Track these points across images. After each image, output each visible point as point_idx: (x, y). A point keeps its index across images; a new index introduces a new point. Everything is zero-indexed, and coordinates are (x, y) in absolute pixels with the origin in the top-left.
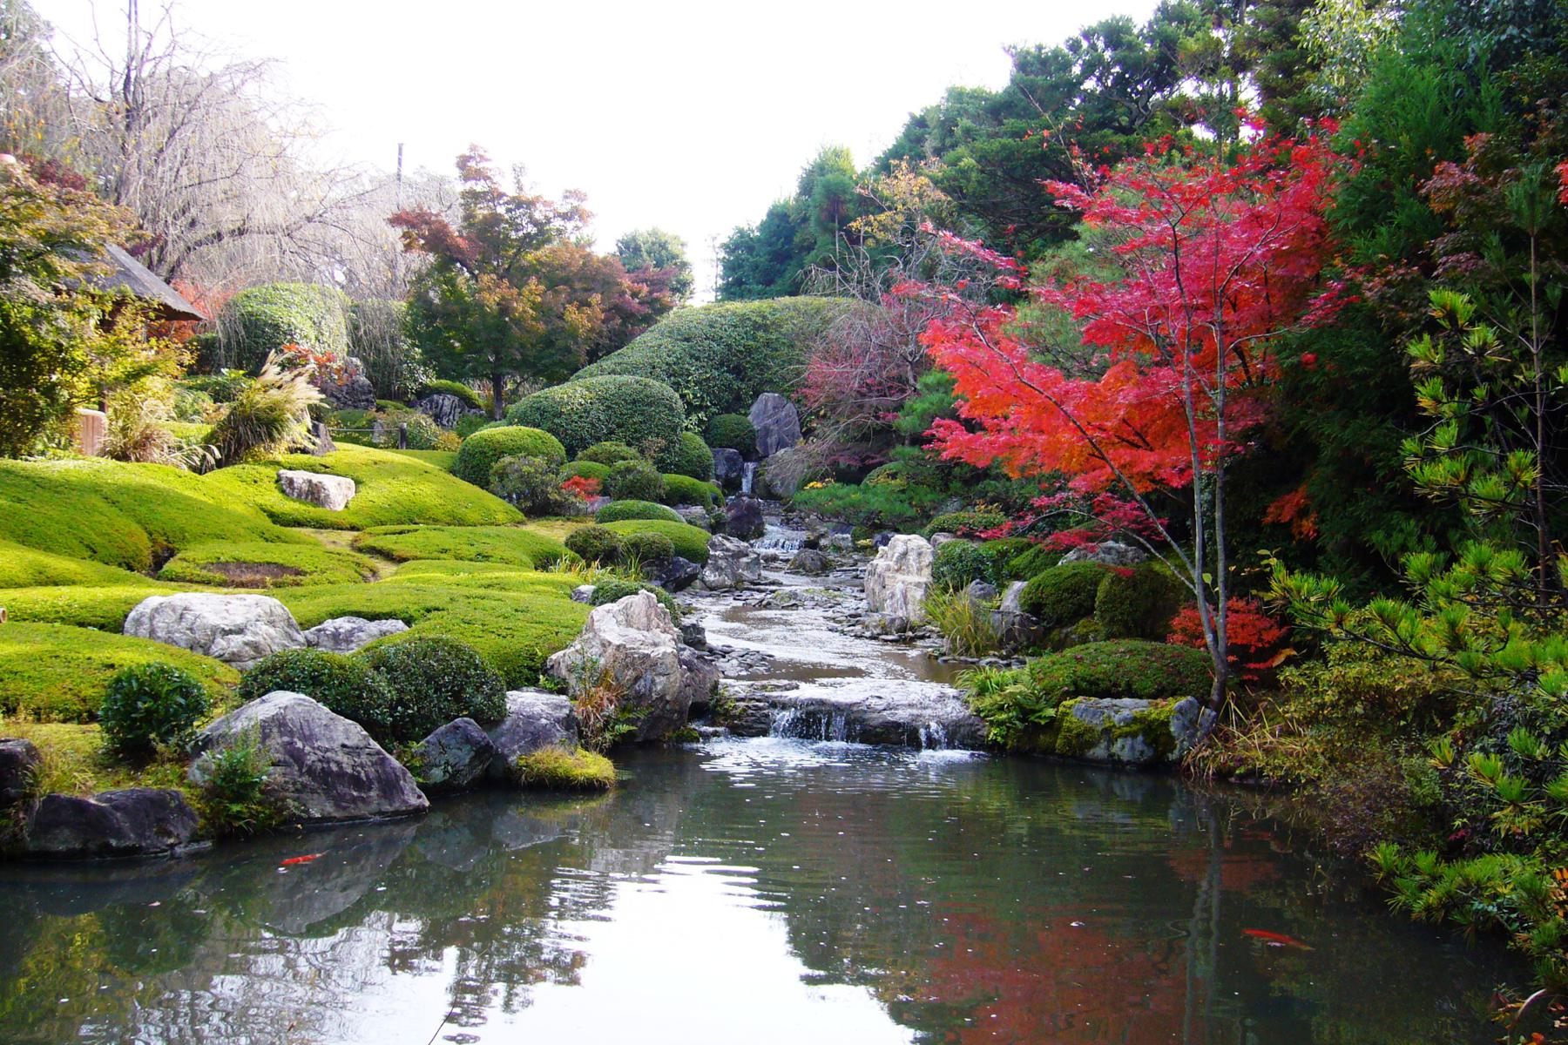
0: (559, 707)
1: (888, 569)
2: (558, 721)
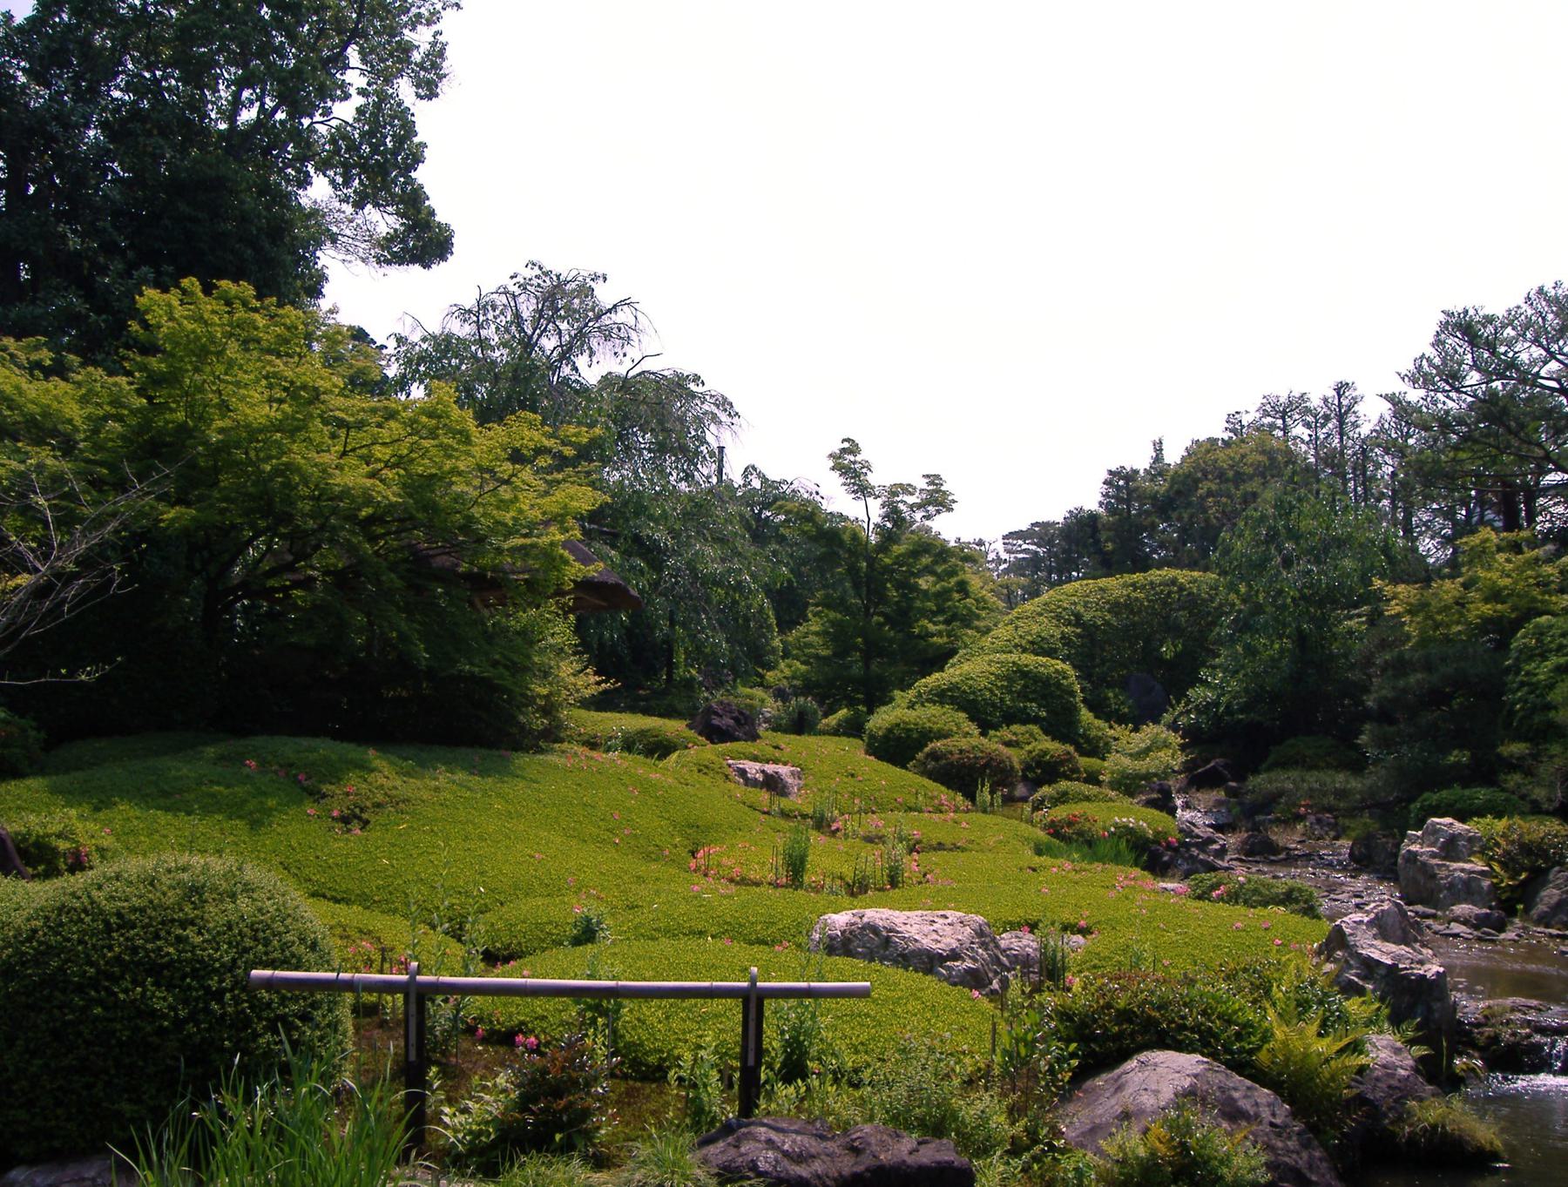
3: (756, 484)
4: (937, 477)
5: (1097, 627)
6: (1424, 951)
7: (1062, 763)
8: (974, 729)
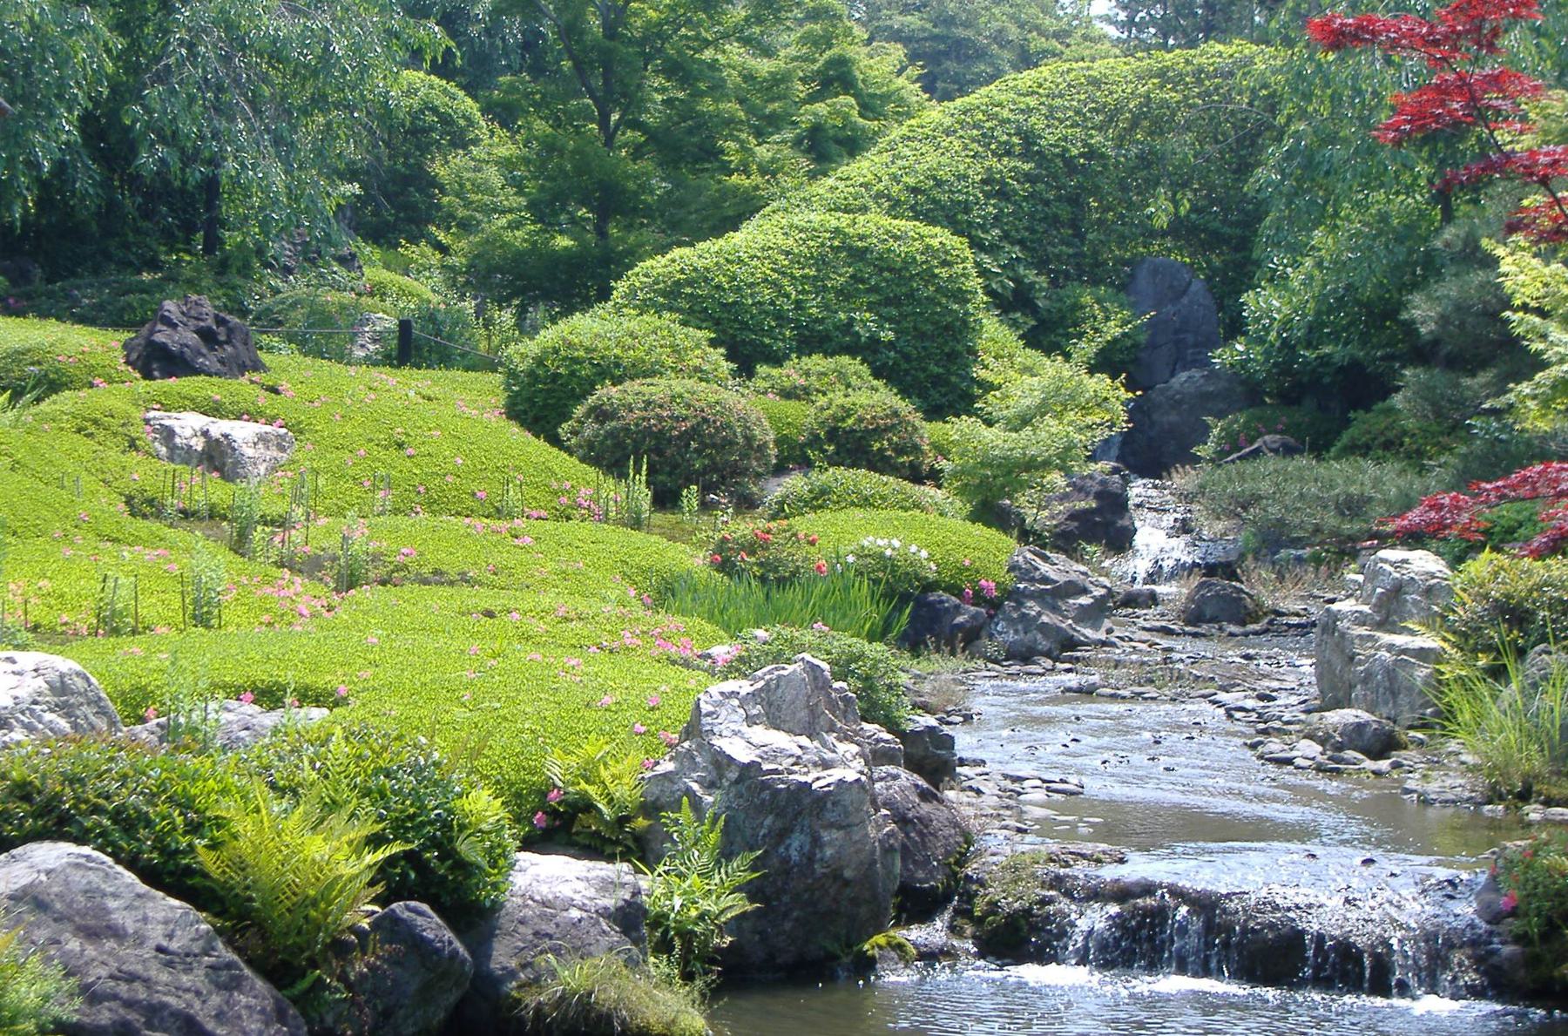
0: (607, 886)
1: (1361, 620)
2: (605, 913)
5: (1069, 162)
7: (879, 432)
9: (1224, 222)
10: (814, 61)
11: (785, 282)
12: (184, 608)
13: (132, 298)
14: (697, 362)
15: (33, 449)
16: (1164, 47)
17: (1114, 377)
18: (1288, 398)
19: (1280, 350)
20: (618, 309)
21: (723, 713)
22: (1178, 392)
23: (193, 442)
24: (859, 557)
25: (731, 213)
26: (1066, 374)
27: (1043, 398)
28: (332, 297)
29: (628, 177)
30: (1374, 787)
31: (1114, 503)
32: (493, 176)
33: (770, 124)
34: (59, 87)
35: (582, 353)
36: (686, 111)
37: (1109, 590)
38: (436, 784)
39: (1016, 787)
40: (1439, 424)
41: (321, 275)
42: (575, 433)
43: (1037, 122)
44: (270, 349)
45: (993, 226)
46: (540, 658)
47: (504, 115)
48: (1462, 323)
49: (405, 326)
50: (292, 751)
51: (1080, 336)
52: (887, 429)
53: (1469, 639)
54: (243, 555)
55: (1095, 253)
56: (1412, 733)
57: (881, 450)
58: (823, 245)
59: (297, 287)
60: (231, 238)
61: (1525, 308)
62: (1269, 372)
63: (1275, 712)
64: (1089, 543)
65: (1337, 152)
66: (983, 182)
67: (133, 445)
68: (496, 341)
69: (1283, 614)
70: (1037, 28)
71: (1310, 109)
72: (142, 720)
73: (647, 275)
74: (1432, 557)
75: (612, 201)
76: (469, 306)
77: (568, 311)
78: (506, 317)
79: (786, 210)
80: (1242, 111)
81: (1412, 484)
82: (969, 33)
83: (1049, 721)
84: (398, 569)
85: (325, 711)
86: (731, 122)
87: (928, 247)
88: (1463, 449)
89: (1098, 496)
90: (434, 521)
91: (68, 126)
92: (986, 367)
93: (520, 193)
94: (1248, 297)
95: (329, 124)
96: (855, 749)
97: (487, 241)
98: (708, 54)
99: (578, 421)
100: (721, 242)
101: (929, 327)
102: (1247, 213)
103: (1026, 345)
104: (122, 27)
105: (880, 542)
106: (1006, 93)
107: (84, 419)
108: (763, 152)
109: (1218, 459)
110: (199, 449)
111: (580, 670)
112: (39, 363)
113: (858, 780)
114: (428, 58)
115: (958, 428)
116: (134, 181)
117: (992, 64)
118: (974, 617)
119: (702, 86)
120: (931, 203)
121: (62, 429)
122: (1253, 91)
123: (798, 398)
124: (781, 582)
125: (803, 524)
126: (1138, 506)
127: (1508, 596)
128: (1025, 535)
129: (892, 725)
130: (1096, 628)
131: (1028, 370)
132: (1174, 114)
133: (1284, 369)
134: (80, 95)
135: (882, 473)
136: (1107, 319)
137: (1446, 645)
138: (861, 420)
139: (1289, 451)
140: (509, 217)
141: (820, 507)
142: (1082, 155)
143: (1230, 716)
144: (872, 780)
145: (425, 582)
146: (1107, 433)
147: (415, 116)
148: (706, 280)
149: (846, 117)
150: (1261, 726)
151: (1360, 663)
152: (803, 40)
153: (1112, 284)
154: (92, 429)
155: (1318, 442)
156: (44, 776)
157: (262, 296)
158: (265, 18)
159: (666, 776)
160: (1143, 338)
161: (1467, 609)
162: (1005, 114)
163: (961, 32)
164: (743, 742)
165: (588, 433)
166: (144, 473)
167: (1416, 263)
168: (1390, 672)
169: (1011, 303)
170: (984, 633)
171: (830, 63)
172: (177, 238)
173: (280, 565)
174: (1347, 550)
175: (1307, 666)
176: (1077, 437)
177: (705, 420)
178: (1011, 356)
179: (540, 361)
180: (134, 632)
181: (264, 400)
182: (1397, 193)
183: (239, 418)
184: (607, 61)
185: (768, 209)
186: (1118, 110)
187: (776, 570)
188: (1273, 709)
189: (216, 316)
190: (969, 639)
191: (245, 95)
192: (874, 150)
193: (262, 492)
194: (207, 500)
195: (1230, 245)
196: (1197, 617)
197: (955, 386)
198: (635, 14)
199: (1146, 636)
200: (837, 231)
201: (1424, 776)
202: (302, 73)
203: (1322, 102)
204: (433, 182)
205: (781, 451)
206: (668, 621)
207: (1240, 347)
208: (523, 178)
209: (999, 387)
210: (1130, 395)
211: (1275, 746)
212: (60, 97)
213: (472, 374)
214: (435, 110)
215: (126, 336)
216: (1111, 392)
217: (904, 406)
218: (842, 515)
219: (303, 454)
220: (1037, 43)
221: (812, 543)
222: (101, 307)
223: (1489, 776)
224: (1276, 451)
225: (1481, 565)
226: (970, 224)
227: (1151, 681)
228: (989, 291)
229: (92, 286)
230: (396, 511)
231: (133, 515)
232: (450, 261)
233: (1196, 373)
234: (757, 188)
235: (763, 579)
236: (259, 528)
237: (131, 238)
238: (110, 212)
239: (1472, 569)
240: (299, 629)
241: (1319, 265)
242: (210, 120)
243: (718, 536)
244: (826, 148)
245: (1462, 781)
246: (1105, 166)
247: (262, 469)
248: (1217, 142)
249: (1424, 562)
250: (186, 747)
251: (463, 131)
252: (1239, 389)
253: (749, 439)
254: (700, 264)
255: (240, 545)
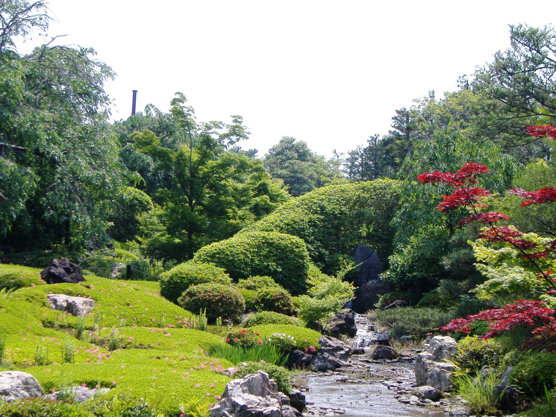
1: (429, 358)
3: (154, 114)
4: (240, 117)
5: (335, 216)
6: (272, 400)
7: (277, 300)
8: (227, 278)
9: (383, 234)
10: (256, 184)
11: (248, 253)
12: (62, 357)
13: (43, 258)
14: (221, 278)
15: (13, 306)
16: (362, 180)
17: (350, 283)
18: (403, 289)
19: (401, 274)
20: (196, 262)
21: (235, 389)
22: (369, 287)
23: (63, 304)
24: (272, 339)
25: (230, 231)
26: (336, 282)
27: (329, 289)
28: (105, 258)
29: (199, 220)
30: (435, 410)
31: (350, 322)
32: (155, 220)
33: (242, 204)
34: (20, 192)
35: (185, 275)
36: (216, 200)
37: (350, 349)
38: (147, 413)
39: (324, 411)
40: (451, 296)
41: (102, 251)
42: (182, 300)
43: (325, 203)
44: (86, 274)
45: (312, 236)
46: (176, 372)
47: (159, 201)
48: (458, 265)
49: (129, 267)
50: (101, 403)
51: (340, 269)
52: (280, 299)
53: (463, 364)
54: (80, 339)
55: (343, 244)
56: (446, 393)
57: (278, 305)
58: (259, 242)
59: (94, 255)
60: (74, 239)
61: (481, 262)
62: (397, 281)
63: (403, 387)
64: (343, 334)
65: (418, 213)
66: (309, 222)
67: (44, 304)
68: (156, 271)
69: (403, 356)
70: (322, 174)
71: (409, 199)
72: (51, 392)
73: (204, 251)
74: (451, 338)
75: (193, 228)
76: (148, 260)
77: (179, 262)
78: (159, 264)
79: (247, 231)
80: (388, 200)
81: (443, 315)
82: (301, 176)
83: (333, 390)
84: (129, 344)
85: (109, 389)
86: (230, 203)
87: (292, 242)
88: (459, 305)
89: (345, 319)
90: (139, 329)
91: (22, 205)
92: (310, 280)
93: (164, 225)
94: (390, 257)
95: (104, 204)
96: (276, 400)
97: (154, 240)
98: (223, 182)
99: (184, 296)
100: (228, 240)
101: (293, 267)
102: (390, 231)
103: (322, 273)
104: (39, 173)
105: (279, 334)
106: (315, 195)
107: (29, 296)
108: (240, 213)
109: (382, 308)
110: (65, 306)
111: (188, 376)
112: (14, 279)
113: (277, 410)
114: (135, 183)
115: (302, 299)
116: (43, 222)
117: (308, 185)
118: (308, 358)
119: (221, 192)
120: (293, 229)
121: (22, 300)
122: (392, 194)
123: (252, 289)
124: (249, 347)
125: (256, 329)
126: (358, 322)
127: (475, 350)
128: (323, 332)
129: (286, 393)
130: (346, 360)
131: (323, 280)
132: (367, 201)
133: (402, 279)
134: (26, 195)
135: (279, 313)
136: (348, 264)
137: (456, 366)
138: (272, 296)
139: (404, 305)
140: (160, 233)
141: (260, 323)
142: (339, 213)
143: (389, 388)
144: (282, 410)
145: (137, 348)
146: (348, 300)
147: (131, 201)
148: (223, 252)
149: (266, 202)
150: (399, 391)
151: (429, 371)
152: (252, 178)
153: (348, 253)
154: (31, 300)
155: (412, 301)
156: (23, 411)
157: (83, 257)
158: (85, 171)
159: (217, 410)
160: (358, 270)
161: (462, 354)
162: (315, 201)
163: (299, 175)
164: (241, 398)
165: (187, 300)
166: (48, 313)
167: (442, 247)
168: (439, 374)
169: (317, 259)
170: (311, 363)
171: (260, 185)
172: (57, 239)
173: (92, 343)
174: (423, 336)
175: (412, 373)
176: (339, 301)
177: (224, 296)
178: (318, 276)
179: (171, 278)
180: (47, 364)
181: (85, 290)
182: (436, 225)
183: (77, 296)
184: (192, 183)
185: (242, 230)
186: (350, 199)
187: (246, 343)
188: (402, 385)
189: (70, 264)
190: (306, 365)
191: (78, 195)
192: (275, 212)
193: (85, 319)
194: (68, 320)
195: (385, 241)
196: (377, 357)
197: (300, 286)
198: (200, 170)
199: (361, 363)
200: (264, 237)
201: (450, 407)
202: (96, 188)
203: (413, 197)
204: (137, 222)
205: (247, 306)
206: (214, 360)
207: (388, 273)
208: (165, 221)
209: (314, 286)
210: (355, 288)
211: (404, 398)
212: (20, 195)
213: (150, 282)
214: (137, 199)
215: (41, 270)
216: (350, 288)
217: (285, 292)
218: (267, 326)
219: (98, 307)
220: (323, 178)
221: (258, 335)
222: (33, 261)
223: (471, 406)
224: (400, 305)
225: (466, 341)
226: (305, 235)
227: (364, 378)
228: (310, 256)
229: (29, 254)
230: (127, 325)
231: (45, 326)
232: (142, 246)
233: (374, 281)
234: (238, 224)
235: (243, 346)
236: (85, 331)
237: (42, 239)
238: (35, 231)
239: (463, 342)
240: (99, 363)
241: (412, 247)
242: (67, 202)
243: (228, 333)
244: (260, 211)
245: (462, 408)
246: (346, 217)
247: (85, 312)
248: (380, 209)
249: (448, 340)
250: (68, 401)
251: (146, 206)
252: (388, 286)
253: (237, 302)
254: (221, 247)
255: (78, 336)
